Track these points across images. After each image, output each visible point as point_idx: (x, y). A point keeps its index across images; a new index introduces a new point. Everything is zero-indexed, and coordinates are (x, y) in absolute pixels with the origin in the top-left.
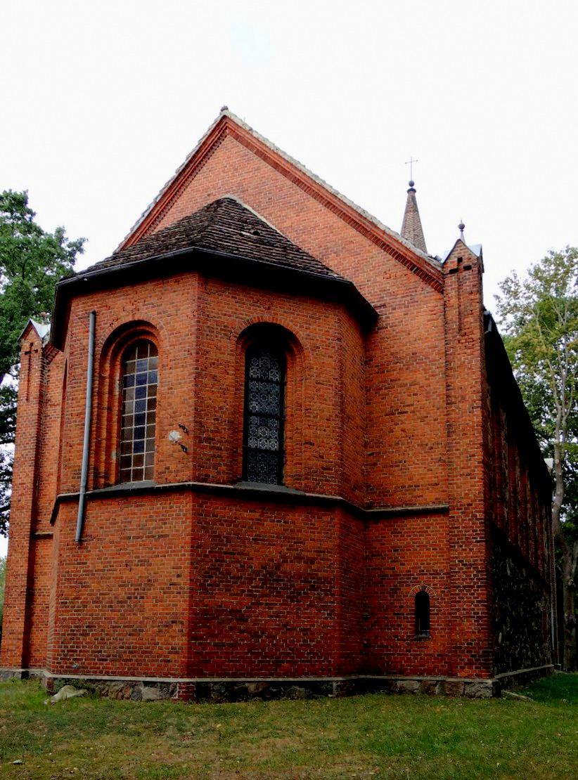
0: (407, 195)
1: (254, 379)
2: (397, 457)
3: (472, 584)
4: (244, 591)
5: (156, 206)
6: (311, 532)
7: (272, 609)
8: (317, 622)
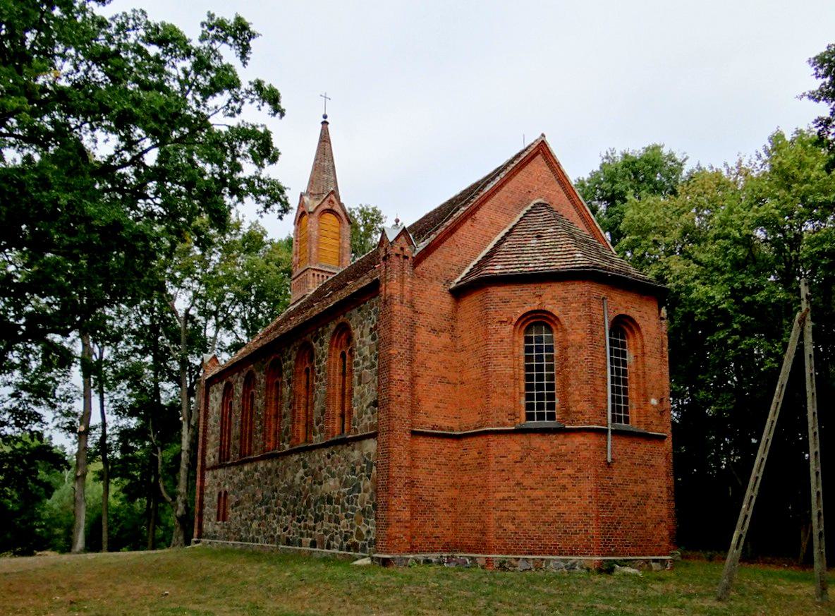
0: (321, 126)
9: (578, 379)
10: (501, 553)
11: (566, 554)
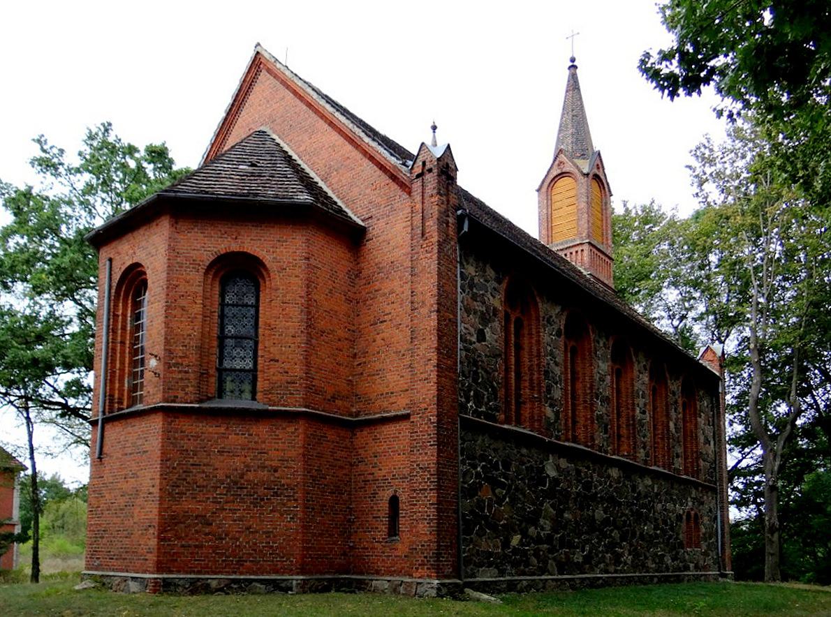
1: (231, 305)
2: (378, 366)
3: (426, 487)
4: (209, 498)
5: (212, 147)
6: (275, 443)
7: (236, 513)
8: (280, 525)
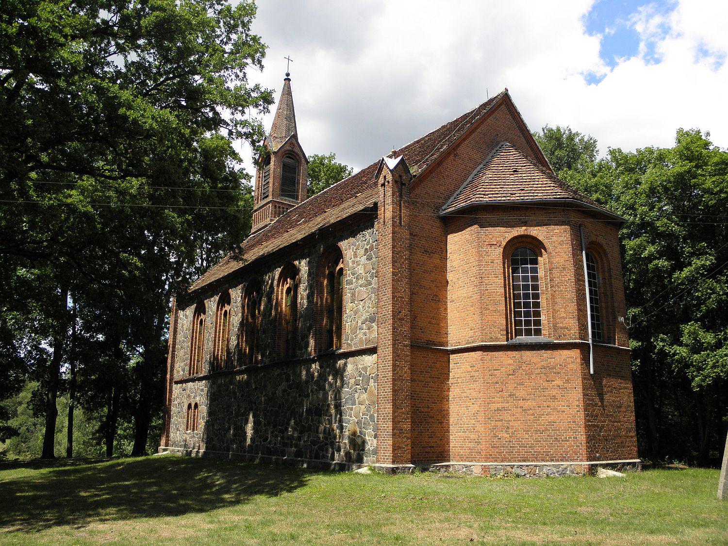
9: (563, 298)
10: (496, 461)
11: (557, 461)
